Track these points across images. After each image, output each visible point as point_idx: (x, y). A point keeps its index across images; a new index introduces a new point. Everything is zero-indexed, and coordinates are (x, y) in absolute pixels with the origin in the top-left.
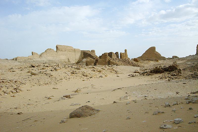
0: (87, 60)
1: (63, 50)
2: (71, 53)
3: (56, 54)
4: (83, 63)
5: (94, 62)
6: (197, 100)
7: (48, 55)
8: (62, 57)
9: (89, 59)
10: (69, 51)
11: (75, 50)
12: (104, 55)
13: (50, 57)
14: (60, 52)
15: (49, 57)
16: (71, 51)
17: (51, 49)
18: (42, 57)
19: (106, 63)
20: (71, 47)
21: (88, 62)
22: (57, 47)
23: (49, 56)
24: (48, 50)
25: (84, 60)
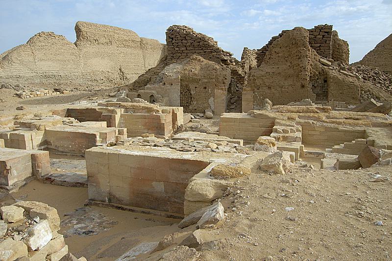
0: (188, 67)
1: (103, 40)
2: (129, 50)
3: (74, 51)
4: (168, 86)
5: (228, 82)
6: (390, 153)
7: (39, 55)
8: (100, 64)
9: (197, 66)
10: (125, 43)
11: (142, 44)
12: (286, 45)
13: (50, 63)
14: (88, 48)
15: (43, 63)
16: (131, 44)
17: (51, 35)
18: (11, 62)
19: (303, 86)
20: (130, 31)
21: (196, 81)
22: (78, 30)
23: (41, 60)
24: (41, 39)
25: (174, 70)
